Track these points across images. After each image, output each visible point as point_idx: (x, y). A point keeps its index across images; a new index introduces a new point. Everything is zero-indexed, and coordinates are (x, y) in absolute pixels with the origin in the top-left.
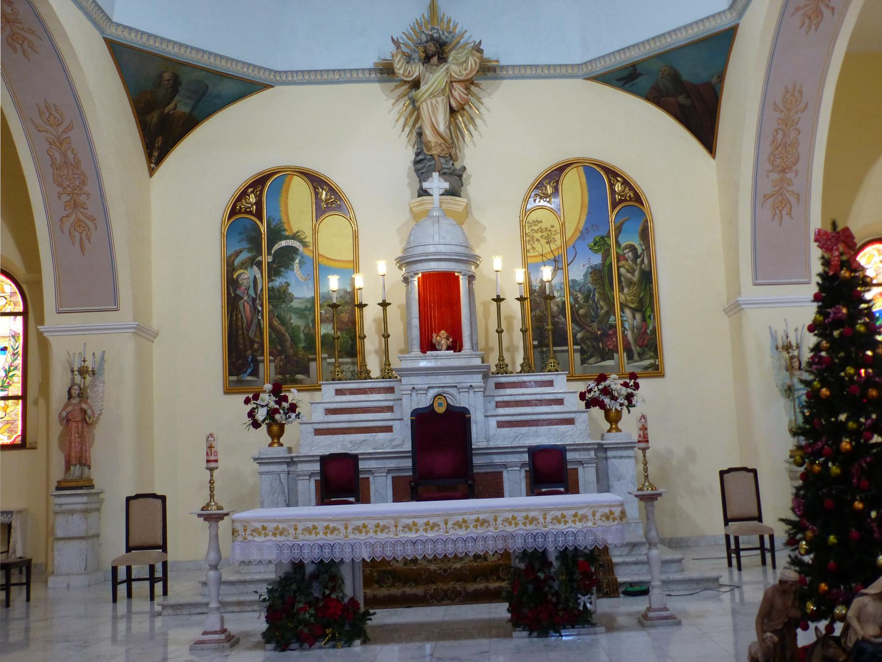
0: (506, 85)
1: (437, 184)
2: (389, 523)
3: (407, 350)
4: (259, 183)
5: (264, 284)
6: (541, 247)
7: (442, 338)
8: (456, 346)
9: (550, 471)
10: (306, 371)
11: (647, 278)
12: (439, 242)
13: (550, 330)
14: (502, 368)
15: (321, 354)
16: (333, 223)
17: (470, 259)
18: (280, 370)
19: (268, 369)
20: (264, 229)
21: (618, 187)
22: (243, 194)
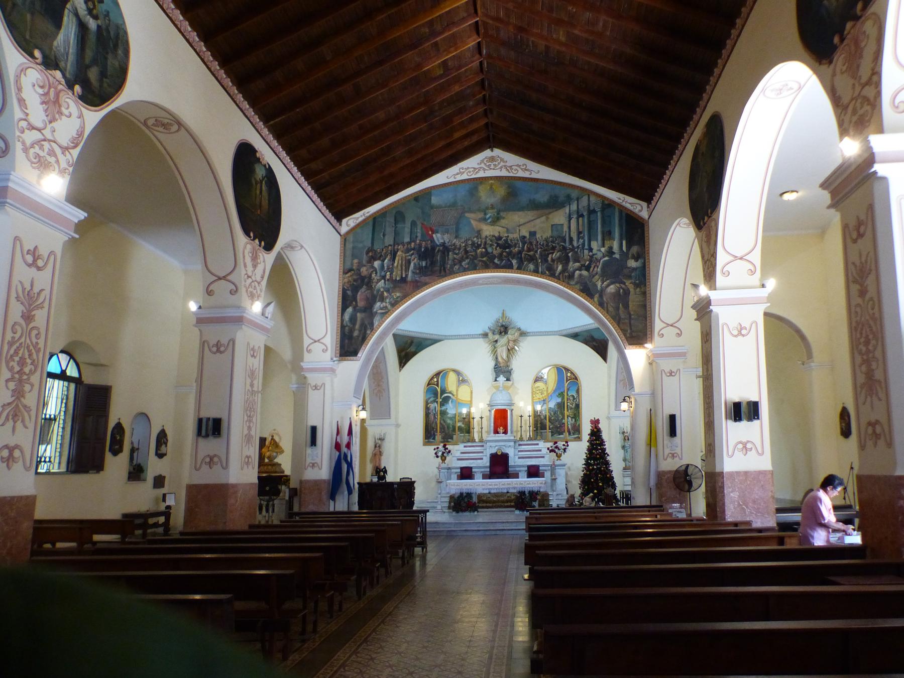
0: (529, 338)
1: (502, 379)
2: (480, 485)
3: (488, 432)
4: (438, 374)
5: (438, 409)
6: (539, 396)
7: (501, 430)
8: (505, 432)
9: (534, 472)
10: (452, 438)
11: (578, 406)
12: (501, 401)
13: (540, 425)
14: (521, 439)
15: (457, 432)
16: (464, 389)
17: (511, 404)
18: (443, 438)
19: (439, 437)
20: (439, 390)
21: (569, 374)
22: (432, 378)
